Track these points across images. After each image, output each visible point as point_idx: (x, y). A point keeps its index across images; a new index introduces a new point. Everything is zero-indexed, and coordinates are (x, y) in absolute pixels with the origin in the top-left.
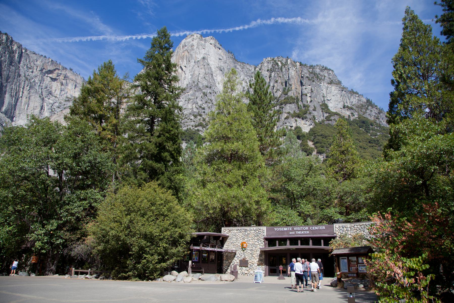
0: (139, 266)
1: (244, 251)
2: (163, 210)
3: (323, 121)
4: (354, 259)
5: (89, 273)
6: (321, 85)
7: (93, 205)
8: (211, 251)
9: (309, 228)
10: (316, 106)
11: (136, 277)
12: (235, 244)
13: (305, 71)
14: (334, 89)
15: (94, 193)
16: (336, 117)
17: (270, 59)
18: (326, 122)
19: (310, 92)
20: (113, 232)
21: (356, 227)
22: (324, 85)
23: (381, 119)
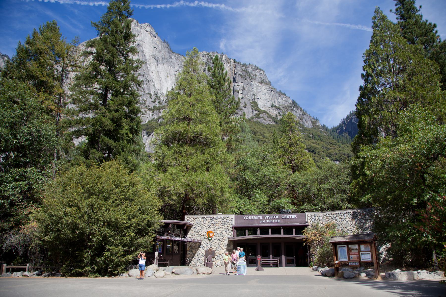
0: (100, 260)
1: (210, 240)
2: (128, 193)
3: (252, 118)
4: (356, 246)
5: (27, 270)
6: (252, 83)
7: (33, 186)
8: (175, 241)
9: (280, 217)
10: (246, 103)
11: (94, 272)
12: (200, 233)
13: (239, 68)
14: (264, 88)
15: (32, 171)
16: (265, 115)
17: (205, 53)
18: (255, 120)
19: (242, 89)
20: (69, 219)
21: (328, 215)
22: (255, 84)
23: (304, 121)
